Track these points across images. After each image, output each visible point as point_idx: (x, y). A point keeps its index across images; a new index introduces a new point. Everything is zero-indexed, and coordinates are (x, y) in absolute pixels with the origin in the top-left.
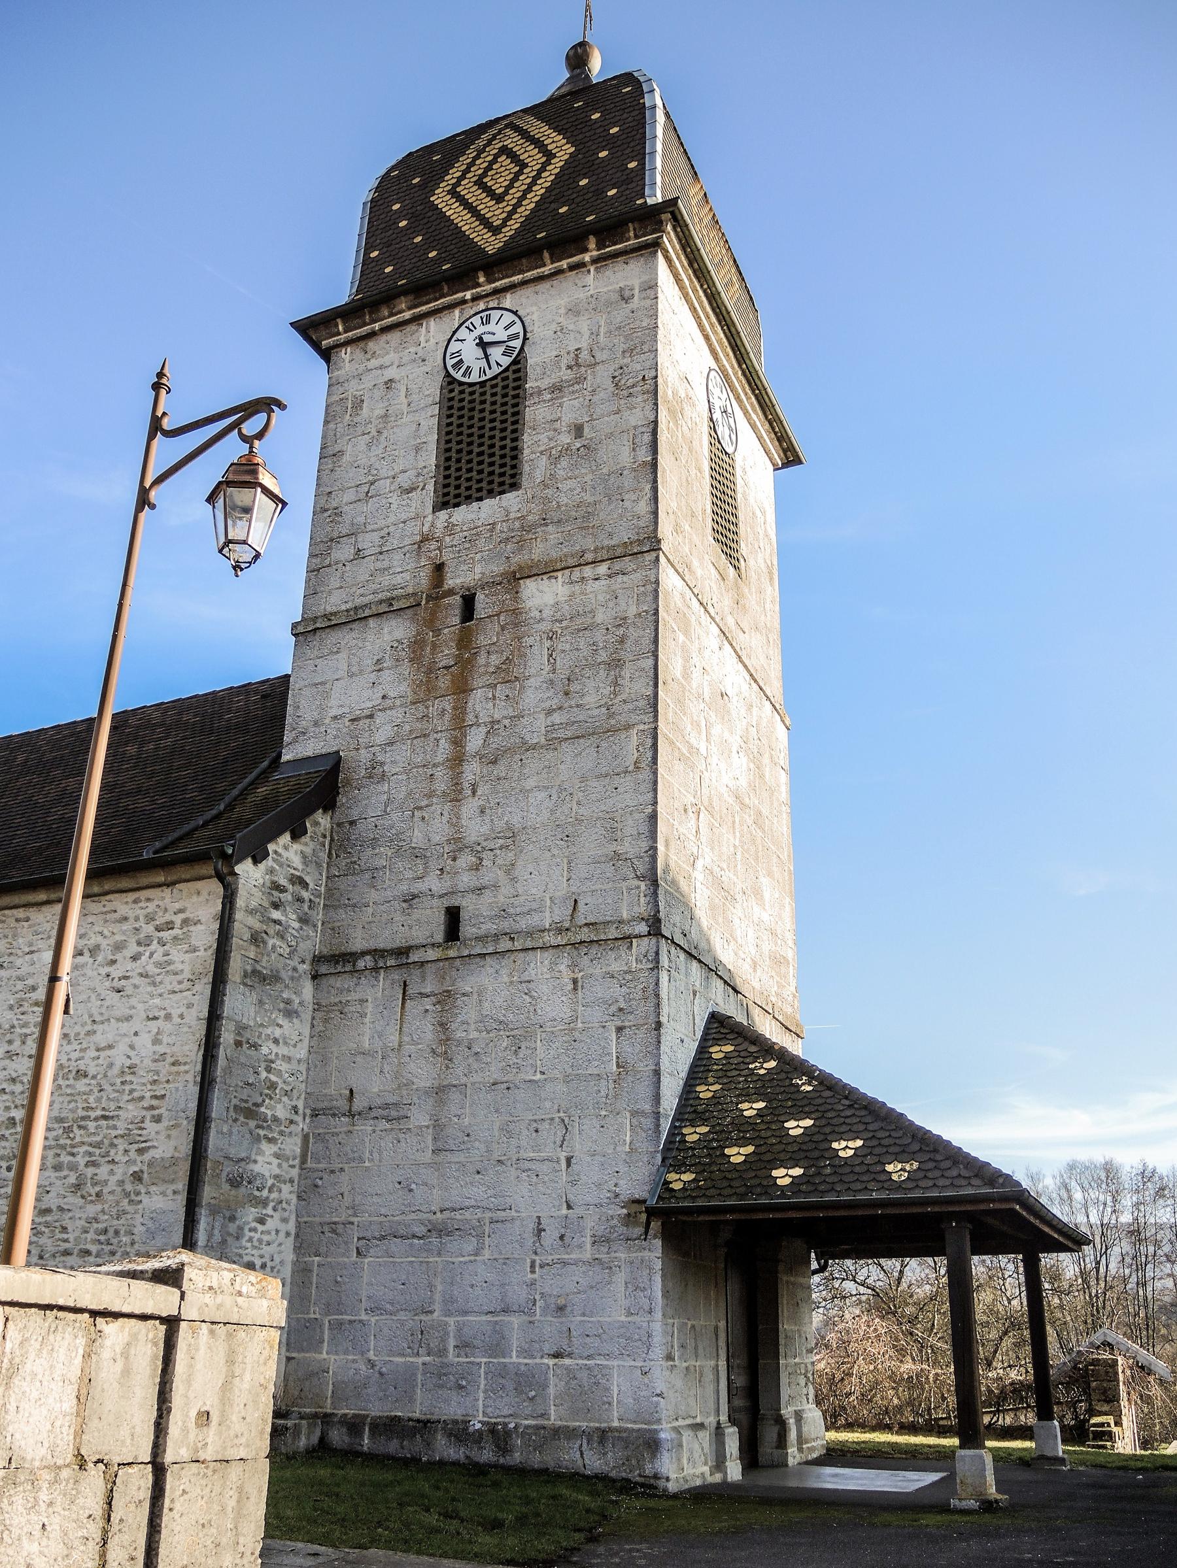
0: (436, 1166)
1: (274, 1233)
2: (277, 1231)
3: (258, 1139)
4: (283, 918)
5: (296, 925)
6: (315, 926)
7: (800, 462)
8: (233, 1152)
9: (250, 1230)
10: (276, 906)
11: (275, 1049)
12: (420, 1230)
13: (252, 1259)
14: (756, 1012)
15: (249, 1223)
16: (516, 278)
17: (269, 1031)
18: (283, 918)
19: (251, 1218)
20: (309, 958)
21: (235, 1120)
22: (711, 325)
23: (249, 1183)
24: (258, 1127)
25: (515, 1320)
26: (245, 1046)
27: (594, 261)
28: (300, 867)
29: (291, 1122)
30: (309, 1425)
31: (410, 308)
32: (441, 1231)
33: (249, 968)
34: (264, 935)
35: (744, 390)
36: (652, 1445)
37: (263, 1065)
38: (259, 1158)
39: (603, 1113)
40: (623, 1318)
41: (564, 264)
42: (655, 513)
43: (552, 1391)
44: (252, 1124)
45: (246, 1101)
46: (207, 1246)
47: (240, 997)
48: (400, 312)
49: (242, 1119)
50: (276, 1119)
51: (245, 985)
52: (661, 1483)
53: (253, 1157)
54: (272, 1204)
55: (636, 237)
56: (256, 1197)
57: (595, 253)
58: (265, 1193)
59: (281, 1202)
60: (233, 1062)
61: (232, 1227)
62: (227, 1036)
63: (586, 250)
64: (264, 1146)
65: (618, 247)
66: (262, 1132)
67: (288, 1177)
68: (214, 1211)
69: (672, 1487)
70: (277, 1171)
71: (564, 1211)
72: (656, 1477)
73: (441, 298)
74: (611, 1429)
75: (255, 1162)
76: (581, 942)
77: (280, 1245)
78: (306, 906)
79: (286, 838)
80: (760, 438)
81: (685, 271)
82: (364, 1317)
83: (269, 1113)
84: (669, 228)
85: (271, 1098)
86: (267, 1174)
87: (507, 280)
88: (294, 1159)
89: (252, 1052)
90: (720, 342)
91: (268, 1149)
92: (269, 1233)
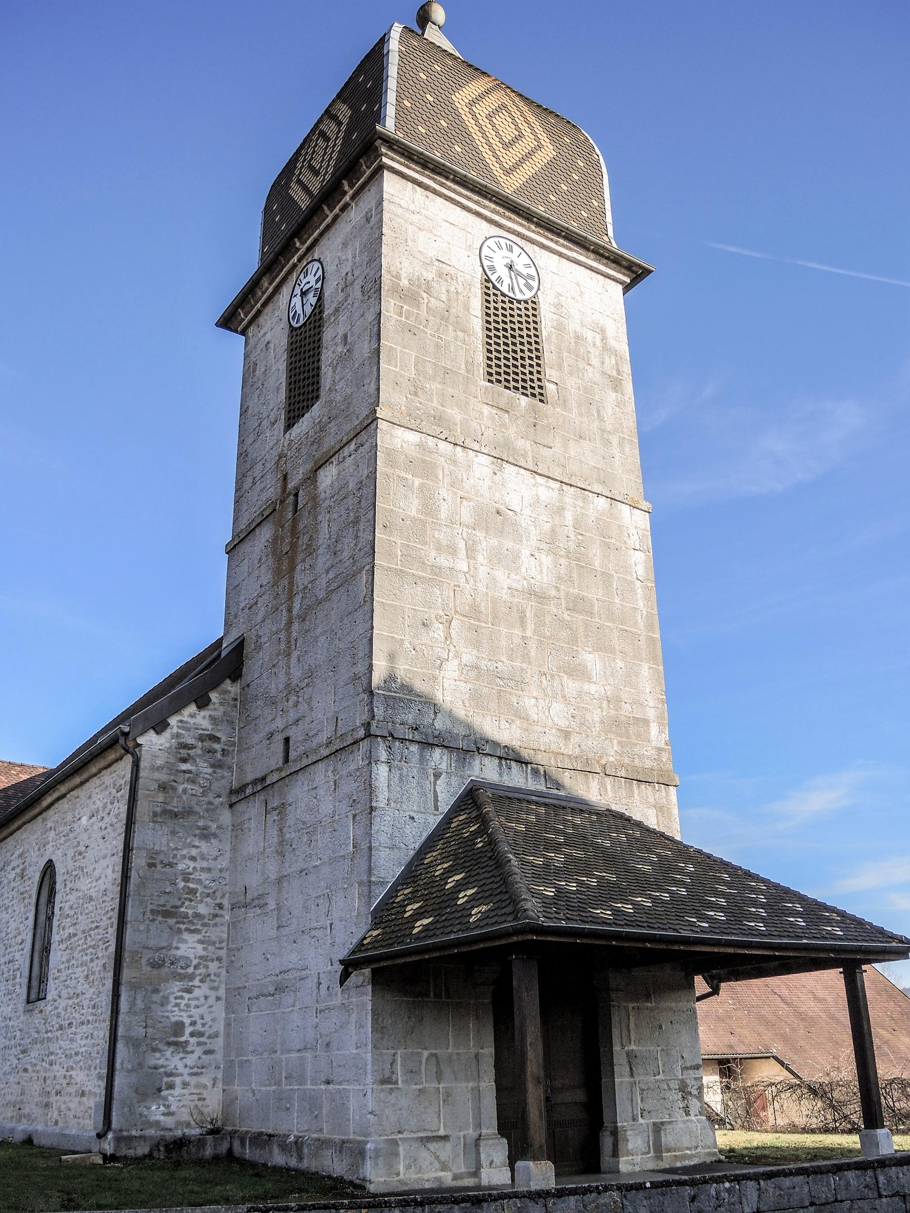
0: (278, 939)
1: (202, 999)
2: (206, 998)
3: (179, 931)
4: (193, 768)
5: (210, 770)
6: (230, 768)
7: (647, 272)
8: (151, 943)
9: (176, 998)
10: (184, 760)
11: (192, 864)
12: (271, 989)
13: (181, 1019)
14: (566, 778)
15: (173, 993)
16: (316, 234)
17: (185, 852)
18: (193, 768)
19: (176, 989)
20: (225, 792)
21: (153, 920)
22: (476, 202)
23: (172, 964)
24: (178, 923)
25: (309, 1055)
26: (159, 867)
27: (353, 198)
28: (210, 727)
29: (216, 916)
30: (215, 1140)
31: (270, 284)
32: (280, 989)
33: (158, 809)
34: (174, 784)
35: (547, 238)
36: (358, 1153)
37: (180, 878)
38: (180, 945)
39: (346, 886)
40: (355, 1051)
41: (337, 210)
42: (378, 389)
43: (325, 1111)
44: (172, 921)
45: (164, 906)
46: (129, 1012)
47: (150, 832)
48: (267, 289)
49: (160, 918)
50: (197, 915)
51: (154, 822)
52: (368, 1185)
53: (175, 945)
54: (198, 978)
55: (368, 168)
56: (180, 974)
57: (351, 192)
58: (190, 970)
59: (209, 975)
60: (145, 878)
61: (156, 998)
62: (138, 861)
63: (345, 193)
64: (186, 936)
65: (362, 180)
66: (183, 927)
67: (215, 957)
68: (134, 987)
69: (372, 1188)
70: (204, 953)
71: (329, 967)
72: (364, 1180)
73: (283, 268)
74: (349, 1141)
75: (177, 948)
76: (337, 751)
77: (211, 1007)
78: (219, 756)
79: (192, 708)
80: (591, 269)
81: (423, 174)
82: (250, 1058)
83: (190, 912)
84: (384, 150)
85: (191, 900)
86: (192, 956)
87: (312, 238)
88: (221, 943)
89: (168, 869)
90: (493, 211)
91: (191, 939)
92: (197, 999)
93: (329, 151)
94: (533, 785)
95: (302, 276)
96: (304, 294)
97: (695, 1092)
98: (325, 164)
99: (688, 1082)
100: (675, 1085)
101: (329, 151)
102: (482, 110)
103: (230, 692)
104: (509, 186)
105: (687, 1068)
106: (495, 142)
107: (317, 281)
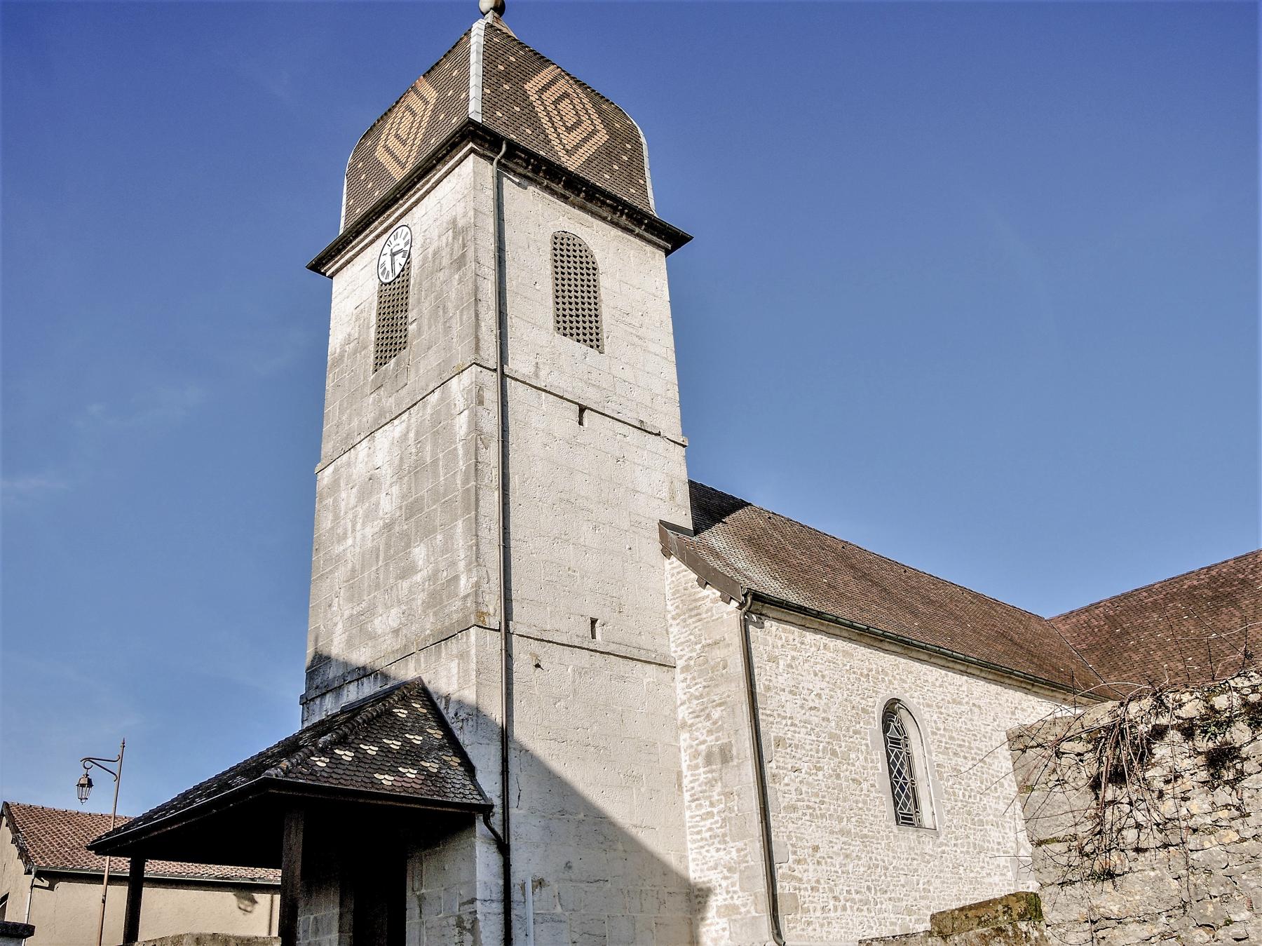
93: (416, 125)
94: (369, 688)
95: (392, 239)
96: (393, 255)
97: (469, 926)
98: (412, 136)
99: (464, 917)
100: (452, 921)
101: (416, 125)
102: (549, 96)
103: (682, 672)
104: (572, 164)
105: (464, 904)
106: (559, 124)
107: (406, 244)
